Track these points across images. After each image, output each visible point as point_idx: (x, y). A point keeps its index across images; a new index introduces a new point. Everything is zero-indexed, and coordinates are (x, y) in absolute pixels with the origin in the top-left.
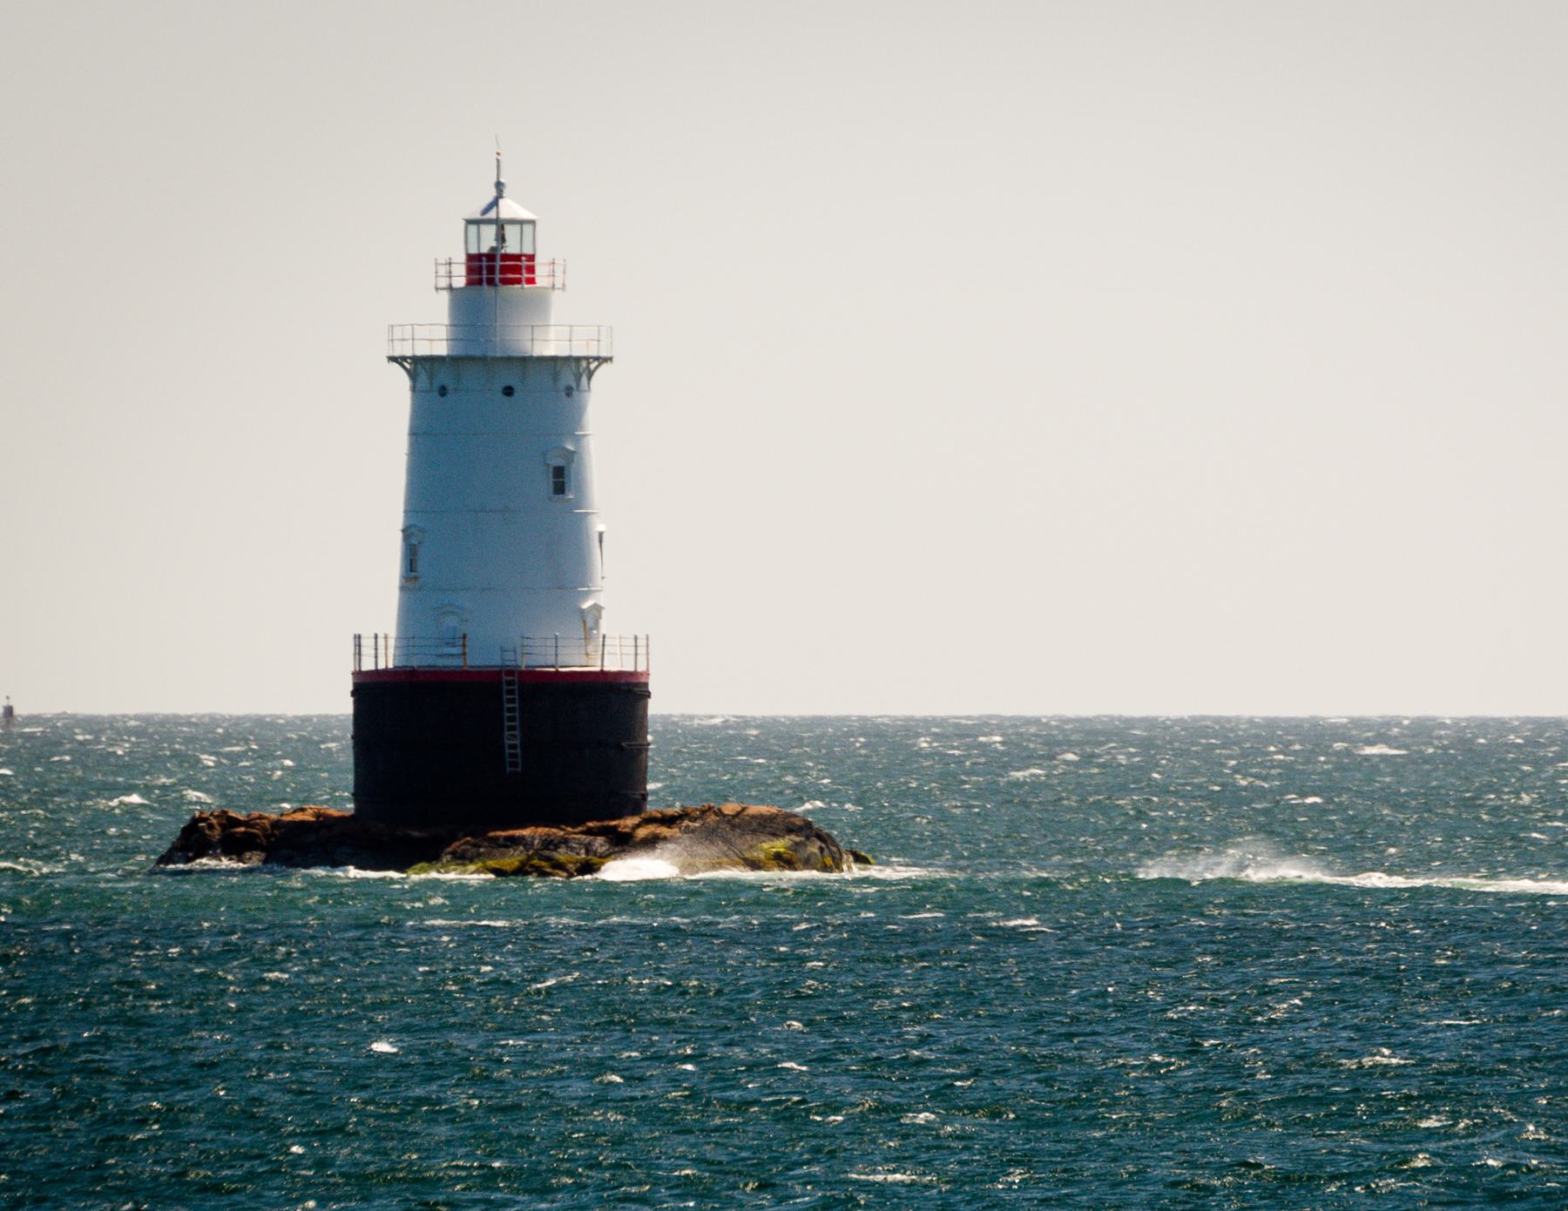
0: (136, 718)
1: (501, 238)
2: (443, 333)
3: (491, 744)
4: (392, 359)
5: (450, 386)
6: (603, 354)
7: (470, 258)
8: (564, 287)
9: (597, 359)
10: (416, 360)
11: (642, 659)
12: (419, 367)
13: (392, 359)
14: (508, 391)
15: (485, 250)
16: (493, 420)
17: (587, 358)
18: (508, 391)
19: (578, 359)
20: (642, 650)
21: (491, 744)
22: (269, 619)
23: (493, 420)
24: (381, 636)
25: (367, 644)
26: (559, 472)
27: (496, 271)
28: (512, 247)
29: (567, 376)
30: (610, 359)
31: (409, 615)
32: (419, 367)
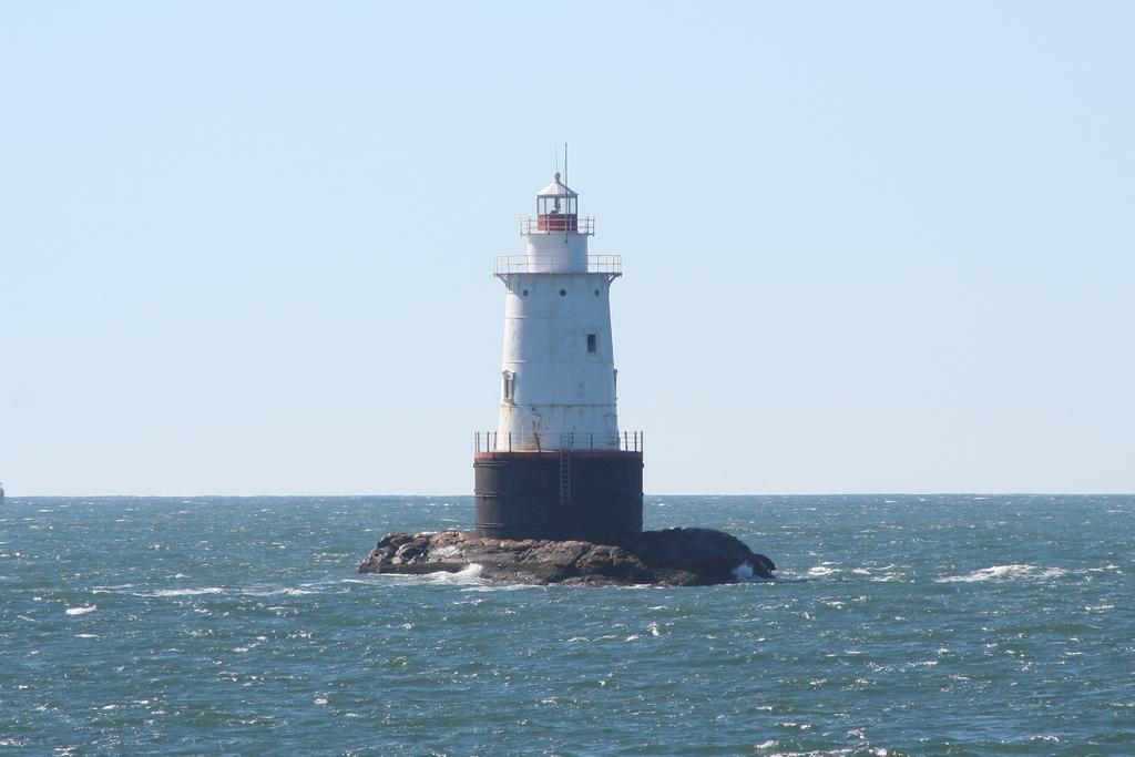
0: (189, 499)
1: (557, 206)
2: (531, 260)
3: (566, 495)
4: (498, 275)
5: (530, 291)
6: (616, 271)
7: (540, 216)
8: (593, 235)
9: (612, 274)
10: (510, 275)
11: (639, 445)
12: (522, 284)
13: (498, 275)
14: (563, 293)
15: (549, 212)
16: (566, 308)
17: (607, 274)
18: (563, 293)
19: (602, 274)
20: (639, 440)
21: (566, 495)
22: (427, 427)
23: (566, 308)
24: (639, 433)
25: (483, 438)
26: (591, 340)
27: (561, 224)
28: (563, 211)
29: (604, 280)
30: (620, 274)
31: (521, 422)
32: (522, 284)
